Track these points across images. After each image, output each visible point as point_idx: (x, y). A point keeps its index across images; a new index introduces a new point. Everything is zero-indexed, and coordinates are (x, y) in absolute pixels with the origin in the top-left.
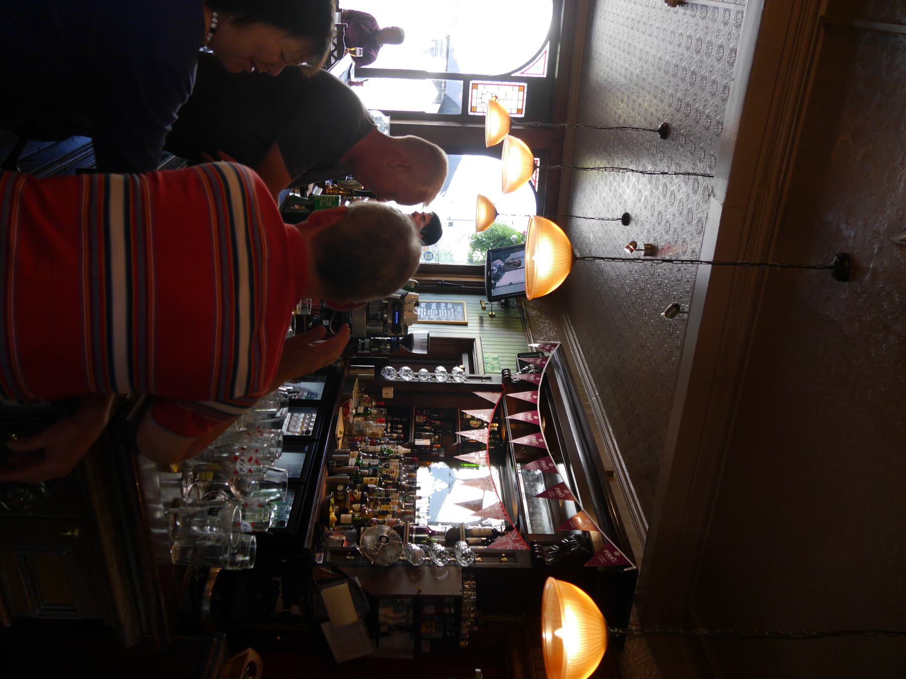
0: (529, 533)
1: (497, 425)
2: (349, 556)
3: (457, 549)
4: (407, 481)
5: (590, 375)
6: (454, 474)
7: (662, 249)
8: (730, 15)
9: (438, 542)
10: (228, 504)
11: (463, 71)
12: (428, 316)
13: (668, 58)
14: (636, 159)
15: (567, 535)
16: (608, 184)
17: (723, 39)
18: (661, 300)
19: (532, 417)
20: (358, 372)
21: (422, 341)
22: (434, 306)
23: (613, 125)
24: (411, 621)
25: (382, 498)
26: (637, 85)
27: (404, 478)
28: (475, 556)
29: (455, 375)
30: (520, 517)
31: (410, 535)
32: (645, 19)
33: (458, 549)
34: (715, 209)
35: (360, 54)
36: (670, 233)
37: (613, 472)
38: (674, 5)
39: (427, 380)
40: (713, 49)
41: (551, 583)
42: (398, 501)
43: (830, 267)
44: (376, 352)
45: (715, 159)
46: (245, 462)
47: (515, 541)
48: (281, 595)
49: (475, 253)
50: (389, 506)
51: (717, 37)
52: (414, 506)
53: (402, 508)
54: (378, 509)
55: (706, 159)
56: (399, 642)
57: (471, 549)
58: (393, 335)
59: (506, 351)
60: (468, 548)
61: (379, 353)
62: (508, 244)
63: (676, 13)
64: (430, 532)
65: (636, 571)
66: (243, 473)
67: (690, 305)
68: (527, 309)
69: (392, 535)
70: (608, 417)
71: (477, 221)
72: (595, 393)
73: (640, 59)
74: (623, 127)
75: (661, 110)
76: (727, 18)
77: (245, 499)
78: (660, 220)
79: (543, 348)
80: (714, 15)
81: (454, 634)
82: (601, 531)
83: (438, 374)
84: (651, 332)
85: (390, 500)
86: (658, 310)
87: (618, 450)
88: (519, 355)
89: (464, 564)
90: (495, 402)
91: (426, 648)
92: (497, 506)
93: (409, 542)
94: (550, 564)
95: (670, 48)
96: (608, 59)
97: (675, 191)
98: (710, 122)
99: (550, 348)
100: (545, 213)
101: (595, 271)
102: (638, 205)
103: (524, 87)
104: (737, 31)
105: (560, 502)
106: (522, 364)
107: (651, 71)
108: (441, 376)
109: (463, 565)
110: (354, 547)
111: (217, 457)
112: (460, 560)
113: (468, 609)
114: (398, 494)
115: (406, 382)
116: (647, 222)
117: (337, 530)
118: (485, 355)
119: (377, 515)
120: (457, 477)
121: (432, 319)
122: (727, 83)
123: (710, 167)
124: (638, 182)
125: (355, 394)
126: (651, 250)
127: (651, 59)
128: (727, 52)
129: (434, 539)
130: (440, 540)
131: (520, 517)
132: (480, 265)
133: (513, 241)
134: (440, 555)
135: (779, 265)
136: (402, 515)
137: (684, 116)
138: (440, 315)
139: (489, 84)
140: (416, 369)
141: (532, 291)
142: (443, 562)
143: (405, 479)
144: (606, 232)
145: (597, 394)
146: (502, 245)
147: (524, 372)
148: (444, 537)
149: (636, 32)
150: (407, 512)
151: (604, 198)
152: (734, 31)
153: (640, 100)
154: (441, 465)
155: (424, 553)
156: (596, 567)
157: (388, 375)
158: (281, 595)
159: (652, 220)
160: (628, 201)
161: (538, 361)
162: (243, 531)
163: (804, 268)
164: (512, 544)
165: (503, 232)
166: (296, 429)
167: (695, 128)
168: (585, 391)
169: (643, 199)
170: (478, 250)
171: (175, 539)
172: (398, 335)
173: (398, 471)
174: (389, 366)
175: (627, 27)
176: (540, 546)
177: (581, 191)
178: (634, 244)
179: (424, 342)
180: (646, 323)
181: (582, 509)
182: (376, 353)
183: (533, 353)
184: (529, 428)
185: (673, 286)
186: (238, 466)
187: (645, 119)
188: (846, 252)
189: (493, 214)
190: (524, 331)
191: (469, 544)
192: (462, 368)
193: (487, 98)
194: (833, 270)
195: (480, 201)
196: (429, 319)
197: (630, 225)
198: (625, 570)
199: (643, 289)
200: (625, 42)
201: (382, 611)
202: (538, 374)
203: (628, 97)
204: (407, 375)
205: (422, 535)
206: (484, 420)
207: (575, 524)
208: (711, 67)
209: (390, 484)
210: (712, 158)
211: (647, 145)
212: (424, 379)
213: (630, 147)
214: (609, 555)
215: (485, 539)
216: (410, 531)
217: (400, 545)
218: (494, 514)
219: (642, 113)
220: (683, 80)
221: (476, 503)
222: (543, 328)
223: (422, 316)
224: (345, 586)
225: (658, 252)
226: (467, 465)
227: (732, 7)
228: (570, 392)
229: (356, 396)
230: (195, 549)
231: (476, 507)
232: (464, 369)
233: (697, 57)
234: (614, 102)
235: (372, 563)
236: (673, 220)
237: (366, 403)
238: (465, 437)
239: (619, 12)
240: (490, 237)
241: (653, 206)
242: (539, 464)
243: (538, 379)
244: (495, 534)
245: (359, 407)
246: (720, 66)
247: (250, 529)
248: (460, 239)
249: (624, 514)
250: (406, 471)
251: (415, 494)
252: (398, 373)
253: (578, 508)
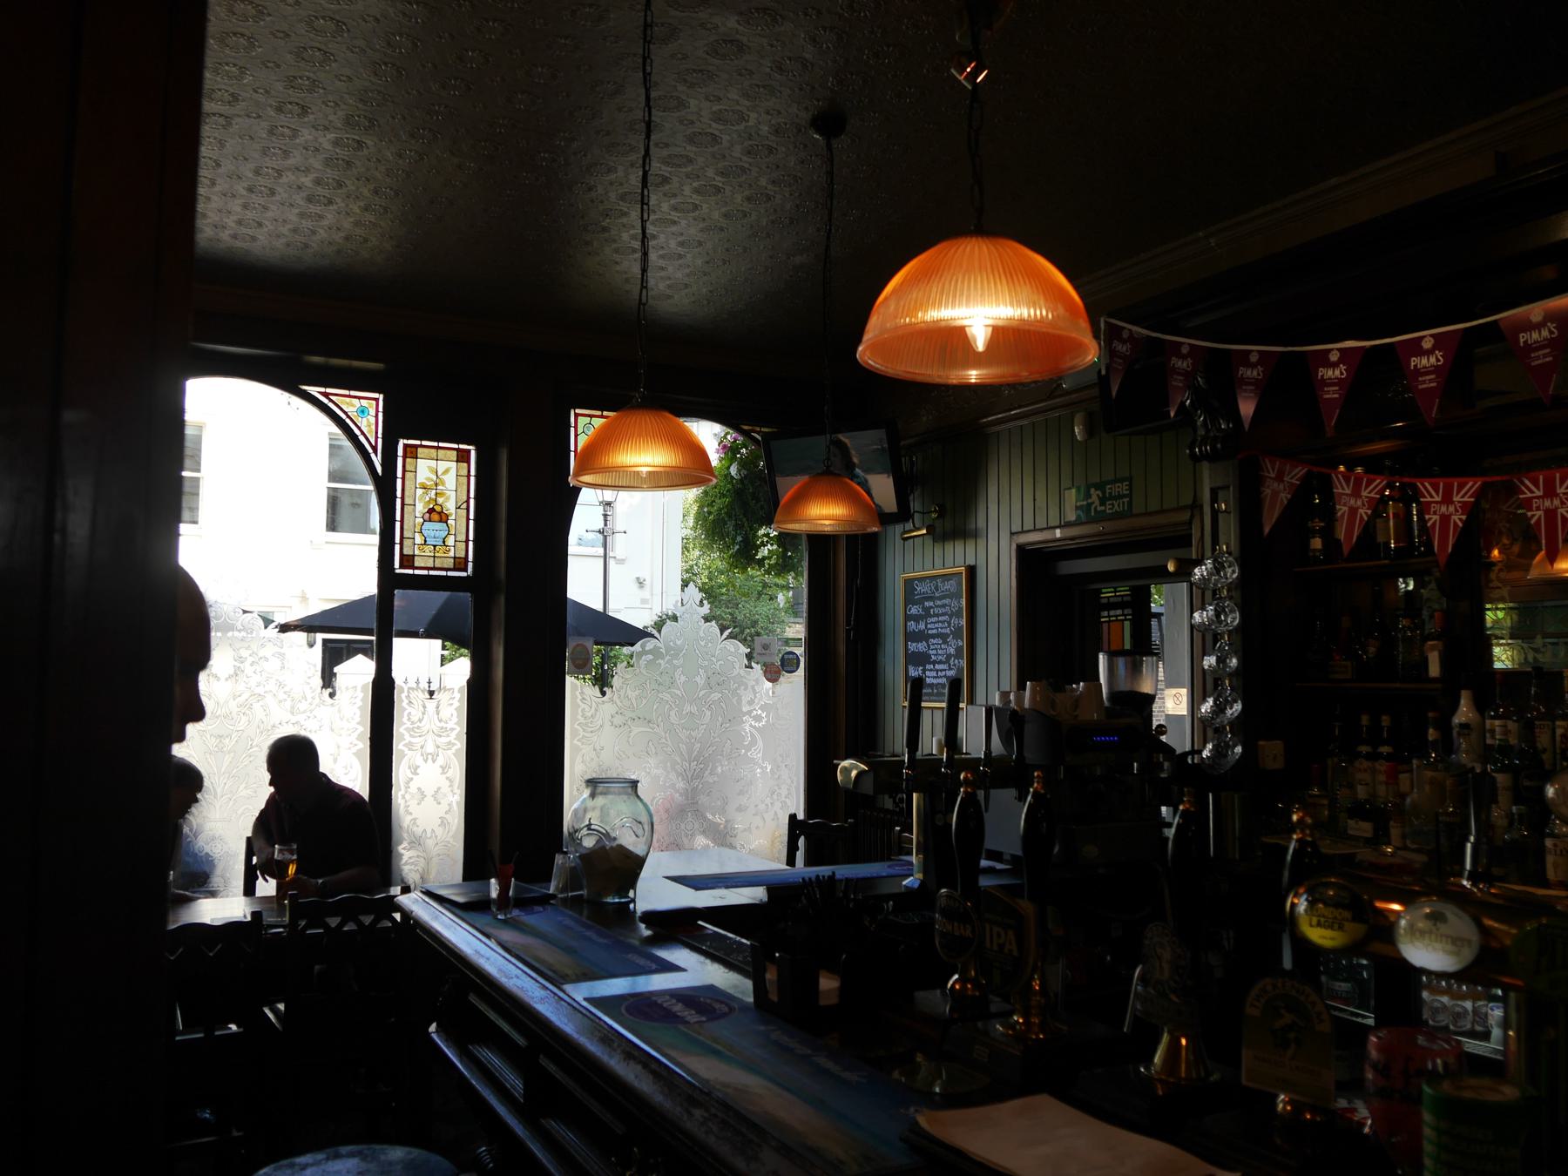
133: (744, 472)
138: (948, 631)
166: (1466, 1010)
207: (1246, 394)
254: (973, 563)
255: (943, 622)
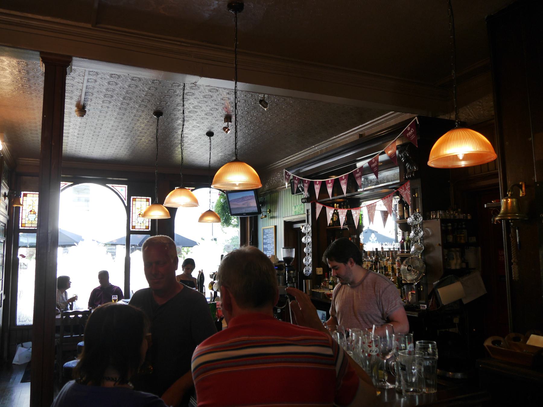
0: (399, 182)
1: (335, 204)
2: (421, 289)
3: (412, 224)
4: (372, 256)
5: (302, 151)
6: (366, 230)
7: (227, 112)
8: (91, 79)
9: (409, 235)
10: (397, 359)
11: (124, 234)
12: (271, 249)
13: (115, 114)
14: (175, 130)
15: (399, 159)
16: (190, 146)
17: (104, 82)
18: (257, 111)
19: (330, 183)
20: (308, 289)
21: (287, 252)
22: (265, 246)
23: (155, 144)
24: (458, 249)
25: (384, 271)
26: (131, 132)
27: (371, 259)
28: (416, 213)
29: (306, 231)
30: (390, 187)
31: (405, 253)
32: (93, 128)
33: (412, 223)
34: (203, 81)
35: (116, 297)
36: (217, 108)
37: (360, 135)
38: (85, 111)
39: (310, 248)
40: (110, 87)
41: (431, 163)
42: (385, 262)
43: (236, 14)
44: (295, 280)
45: (174, 83)
46: (371, 349)
47: (405, 189)
48: (447, 330)
49: (233, 223)
50: (388, 267)
51: (103, 86)
52: (388, 252)
53: (389, 259)
54: (390, 273)
55: (174, 89)
56: (471, 256)
57: (412, 215)
58: (284, 270)
59: (290, 202)
60: (411, 217)
61: (296, 278)
62: (227, 203)
63: (89, 110)
64: (403, 241)
65: (418, 117)
66: (378, 351)
67: (259, 93)
68: (265, 191)
69: (406, 263)
70: (327, 139)
71: (213, 222)
72: (313, 148)
73: (116, 130)
74: (157, 138)
75: (146, 117)
76: (93, 80)
77: (394, 349)
78: (210, 114)
79: (288, 179)
80: (91, 88)
81: (463, 223)
82: (396, 139)
83: (307, 241)
84: (276, 116)
85: (385, 266)
86: (263, 113)
87: (346, 132)
88: (293, 193)
89: (421, 219)
90: (321, 206)
91: (473, 239)
92: (384, 201)
93: (410, 253)
94: (417, 168)
95: (109, 113)
96: (116, 149)
97: (193, 106)
98: (153, 87)
99: (287, 175)
100: (208, 183)
101: (241, 151)
102: (201, 127)
103: (133, 198)
104: (100, 74)
105: (380, 164)
106: (298, 191)
107: (123, 123)
108: (307, 239)
109: (422, 220)
110: (415, 286)
111: (369, 367)
112: (419, 221)
113: (448, 215)
114: (381, 262)
115: (312, 261)
116: (211, 122)
117: (405, 297)
118: (293, 214)
119: (394, 273)
120: (367, 228)
121: (273, 247)
122: (130, 78)
123: (179, 86)
124: (188, 128)
125: (321, 291)
126: (228, 118)
127: (116, 124)
128: (112, 79)
129: (407, 238)
130: (407, 235)
131: (390, 187)
132: (239, 220)
133: (224, 201)
134: (416, 234)
135: (236, 42)
136: (394, 259)
137: (149, 103)
138: (271, 242)
139: (132, 219)
140: (305, 255)
141: (257, 185)
142: (421, 232)
143: (371, 258)
144: (218, 146)
145: (313, 146)
146: (227, 208)
147: (303, 190)
148: (405, 233)
149: (101, 133)
150: (391, 255)
151: (198, 148)
152: (99, 76)
153: (140, 129)
154: (362, 237)
155: (416, 243)
156: (418, 140)
157: (308, 271)
158: (447, 330)
159: (210, 119)
160: (199, 133)
161: (296, 182)
162: (414, 349)
163: (237, 29)
164: (407, 191)
165: (220, 207)
167: (156, 96)
168: (312, 154)
169: (198, 125)
170: (231, 222)
171: (421, 391)
172: (284, 266)
173: (367, 262)
174: (303, 271)
175: (97, 139)
176: (407, 175)
177: (194, 161)
178: (225, 129)
179: (288, 251)
180: (271, 119)
181: (383, 151)
182: (296, 279)
183: (291, 186)
184: (337, 185)
185: (249, 105)
186: (374, 354)
187: (151, 125)
188: (226, 5)
189: (209, 213)
190: (278, 192)
191: (409, 216)
192: (303, 227)
193: (141, 219)
194: (238, 12)
195: (203, 221)
196: (273, 249)
197: (213, 131)
198: (418, 123)
199: (251, 122)
200: (106, 140)
201: (453, 267)
202: (304, 182)
203: (138, 136)
204: (308, 260)
205: (405, 246)
206: (333, 212)
208: (120, 88)
209: (375, 267)
210: (173, 85)
211: (166, 124)
212: (310, 249)
213: (167, 134)
214: (410, 133)
215: (405, 208)
216: (403, 253)
217: (412, 258)
218: (389, 203)
219: (148, 127)
220: (128, 104)
221: (383, 215)
222: (276, 181)
223: (272, 253)
224: (440, 291)
225: (229, 114)
226: (360, 221)
227: (86, 78)
228: (313, 162)
229: (323, 290)
230: (426, 379)
231: (385, 215)
232: (303, 226)
233: (115, 97)
234: (141, 144)
235: (424, 274)
236: (210, 106)
237: (327, 284)
238: (344, 223)
239: (89, 144)
240: (223, 215)
241: (202, 118)
242: (357, 178)
243: (307, 182)
244: (401, 202)
245: (329, 288)
246: (120, 83)
247: (412, 345)
248: (224, 232)
249: (384, 126)
250: (366, 257)
251: (380, 251)
252: (307, 266)
253: (383, 153)
254: (276, 225)
255: (270, 240)
